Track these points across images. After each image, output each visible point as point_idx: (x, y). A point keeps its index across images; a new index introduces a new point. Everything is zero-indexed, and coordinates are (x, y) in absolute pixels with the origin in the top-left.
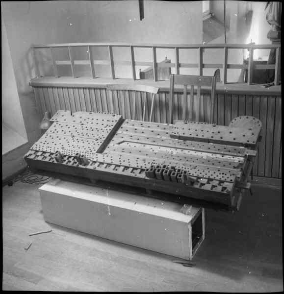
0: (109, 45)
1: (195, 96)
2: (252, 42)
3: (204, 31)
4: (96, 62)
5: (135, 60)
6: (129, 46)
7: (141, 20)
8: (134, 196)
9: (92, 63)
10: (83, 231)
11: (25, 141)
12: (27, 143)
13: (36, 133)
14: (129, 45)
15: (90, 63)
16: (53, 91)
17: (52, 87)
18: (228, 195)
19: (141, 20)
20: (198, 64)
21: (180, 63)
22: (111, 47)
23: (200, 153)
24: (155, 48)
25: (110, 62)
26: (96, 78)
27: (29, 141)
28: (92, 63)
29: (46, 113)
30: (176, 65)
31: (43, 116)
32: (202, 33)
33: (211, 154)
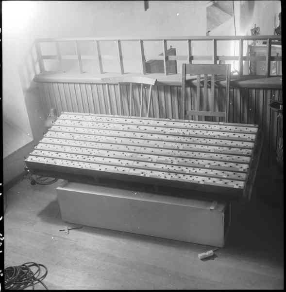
0: (75, 40)
1: (209, 89)
2: (257, 27)
3: (208, 18)
4: (82, 57)
5: (145, 55)
6: (138, 40)
7: (146, 10)
8: (106, 188)
9: (80, 58)
10: (214, 245)
11: (31, 139)
12: (33, 141)
13: (40, 131)
14: (137, 39)
15: (78, 58)
16: (58, 86)
17: (58, 83)
18: (242, 190)
19: (146, 10)
20: (265, 57)
21: (218, 55)
22: (97, 41)
23: (206, 147)
24: (190, 41)
25: (98, 57)
26: (85, 72)
27: (34, 139)
28: (80, 58)
29: (52, 110)
30: (240, 57)
31: (49, 112)
32: (206, 20)
33: (218, 147)
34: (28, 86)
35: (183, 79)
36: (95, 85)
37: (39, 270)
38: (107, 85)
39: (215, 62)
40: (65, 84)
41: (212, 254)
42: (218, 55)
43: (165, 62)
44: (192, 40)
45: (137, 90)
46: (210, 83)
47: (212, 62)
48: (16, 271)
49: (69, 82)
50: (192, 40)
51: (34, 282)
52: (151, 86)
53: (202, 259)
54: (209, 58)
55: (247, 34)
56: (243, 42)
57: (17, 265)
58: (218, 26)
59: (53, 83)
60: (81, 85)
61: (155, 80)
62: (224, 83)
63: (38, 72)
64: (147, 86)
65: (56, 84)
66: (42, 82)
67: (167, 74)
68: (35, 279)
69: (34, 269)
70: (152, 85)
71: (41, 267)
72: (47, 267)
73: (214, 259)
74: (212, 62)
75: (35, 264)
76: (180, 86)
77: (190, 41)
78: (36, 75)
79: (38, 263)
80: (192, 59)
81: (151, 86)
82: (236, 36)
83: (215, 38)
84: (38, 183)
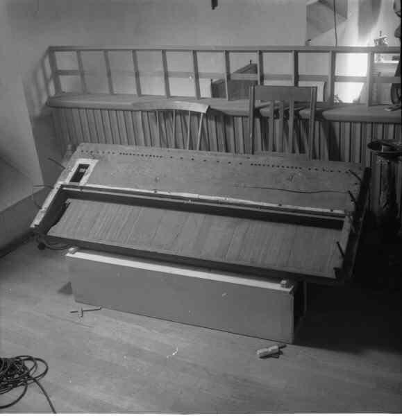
7: (213, 9)
17: (79, 108)
19: (213, 9)
34: (38, 112)
35: (250, 106)
36: (240, 119)
37: (36, 364)
38: (370, 125)
39: (296, 83)
40: (133, 113)
41: (277, 351)
42: (300, 73)
43: (226, 83)
44: (198, 51)
45: (213, 122)
46: (286, 113)
47: (291, 83)
48: (6, 364)
49: (116, 108)
50: (198, 51)
51: (29, 382)
52: (202, 115)
53: (261, 357)
54: (286, 77)
55: (369, 44)
56: (196, 54)
57: (9, 357)
58: (323, 32)
59: (71, 108)
60: (103, 111)
61: (207, 107)
62: (306, 113)
63: (52, 92)
64: (198, 114)
65: (77, 111)
66: (58, 107)
67: (229, 100)
68: (30, 377)
69: (29, 364)
70: (204, 114)
71: (38, 362)
72: (47, 361)
73: (278, 357)
74: (291, 83)
75: (30, 359)
76: (247, 117)
77: (227, 53)
78: (50, 98)
79: (34, 356)
80: (335, 81)
81: (202, 115)
82: (336, 47)
83: (297, 49)
84: (49, 248)
